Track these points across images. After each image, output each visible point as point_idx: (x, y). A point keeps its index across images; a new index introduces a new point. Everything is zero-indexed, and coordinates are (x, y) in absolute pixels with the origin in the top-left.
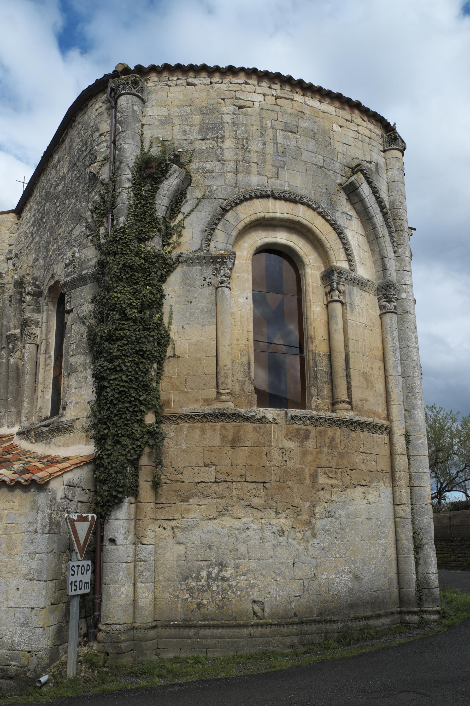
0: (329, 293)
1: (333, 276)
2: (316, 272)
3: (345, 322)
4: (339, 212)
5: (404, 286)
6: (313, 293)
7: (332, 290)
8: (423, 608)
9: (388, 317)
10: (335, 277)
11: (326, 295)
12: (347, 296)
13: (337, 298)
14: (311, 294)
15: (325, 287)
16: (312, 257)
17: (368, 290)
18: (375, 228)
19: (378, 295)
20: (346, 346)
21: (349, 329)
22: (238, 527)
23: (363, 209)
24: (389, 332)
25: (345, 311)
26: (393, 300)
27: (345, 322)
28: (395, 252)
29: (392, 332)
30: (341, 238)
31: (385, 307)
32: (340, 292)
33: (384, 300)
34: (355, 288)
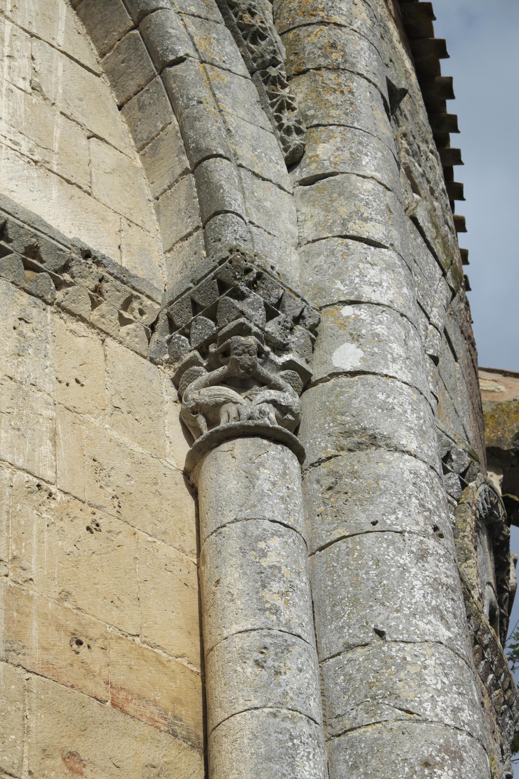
5: (347, 311)
8: (513, 650)
9: (229, 462)
17: (84, 307)
28: (293, 162)
31: (212, 411)
33: (206, 375)
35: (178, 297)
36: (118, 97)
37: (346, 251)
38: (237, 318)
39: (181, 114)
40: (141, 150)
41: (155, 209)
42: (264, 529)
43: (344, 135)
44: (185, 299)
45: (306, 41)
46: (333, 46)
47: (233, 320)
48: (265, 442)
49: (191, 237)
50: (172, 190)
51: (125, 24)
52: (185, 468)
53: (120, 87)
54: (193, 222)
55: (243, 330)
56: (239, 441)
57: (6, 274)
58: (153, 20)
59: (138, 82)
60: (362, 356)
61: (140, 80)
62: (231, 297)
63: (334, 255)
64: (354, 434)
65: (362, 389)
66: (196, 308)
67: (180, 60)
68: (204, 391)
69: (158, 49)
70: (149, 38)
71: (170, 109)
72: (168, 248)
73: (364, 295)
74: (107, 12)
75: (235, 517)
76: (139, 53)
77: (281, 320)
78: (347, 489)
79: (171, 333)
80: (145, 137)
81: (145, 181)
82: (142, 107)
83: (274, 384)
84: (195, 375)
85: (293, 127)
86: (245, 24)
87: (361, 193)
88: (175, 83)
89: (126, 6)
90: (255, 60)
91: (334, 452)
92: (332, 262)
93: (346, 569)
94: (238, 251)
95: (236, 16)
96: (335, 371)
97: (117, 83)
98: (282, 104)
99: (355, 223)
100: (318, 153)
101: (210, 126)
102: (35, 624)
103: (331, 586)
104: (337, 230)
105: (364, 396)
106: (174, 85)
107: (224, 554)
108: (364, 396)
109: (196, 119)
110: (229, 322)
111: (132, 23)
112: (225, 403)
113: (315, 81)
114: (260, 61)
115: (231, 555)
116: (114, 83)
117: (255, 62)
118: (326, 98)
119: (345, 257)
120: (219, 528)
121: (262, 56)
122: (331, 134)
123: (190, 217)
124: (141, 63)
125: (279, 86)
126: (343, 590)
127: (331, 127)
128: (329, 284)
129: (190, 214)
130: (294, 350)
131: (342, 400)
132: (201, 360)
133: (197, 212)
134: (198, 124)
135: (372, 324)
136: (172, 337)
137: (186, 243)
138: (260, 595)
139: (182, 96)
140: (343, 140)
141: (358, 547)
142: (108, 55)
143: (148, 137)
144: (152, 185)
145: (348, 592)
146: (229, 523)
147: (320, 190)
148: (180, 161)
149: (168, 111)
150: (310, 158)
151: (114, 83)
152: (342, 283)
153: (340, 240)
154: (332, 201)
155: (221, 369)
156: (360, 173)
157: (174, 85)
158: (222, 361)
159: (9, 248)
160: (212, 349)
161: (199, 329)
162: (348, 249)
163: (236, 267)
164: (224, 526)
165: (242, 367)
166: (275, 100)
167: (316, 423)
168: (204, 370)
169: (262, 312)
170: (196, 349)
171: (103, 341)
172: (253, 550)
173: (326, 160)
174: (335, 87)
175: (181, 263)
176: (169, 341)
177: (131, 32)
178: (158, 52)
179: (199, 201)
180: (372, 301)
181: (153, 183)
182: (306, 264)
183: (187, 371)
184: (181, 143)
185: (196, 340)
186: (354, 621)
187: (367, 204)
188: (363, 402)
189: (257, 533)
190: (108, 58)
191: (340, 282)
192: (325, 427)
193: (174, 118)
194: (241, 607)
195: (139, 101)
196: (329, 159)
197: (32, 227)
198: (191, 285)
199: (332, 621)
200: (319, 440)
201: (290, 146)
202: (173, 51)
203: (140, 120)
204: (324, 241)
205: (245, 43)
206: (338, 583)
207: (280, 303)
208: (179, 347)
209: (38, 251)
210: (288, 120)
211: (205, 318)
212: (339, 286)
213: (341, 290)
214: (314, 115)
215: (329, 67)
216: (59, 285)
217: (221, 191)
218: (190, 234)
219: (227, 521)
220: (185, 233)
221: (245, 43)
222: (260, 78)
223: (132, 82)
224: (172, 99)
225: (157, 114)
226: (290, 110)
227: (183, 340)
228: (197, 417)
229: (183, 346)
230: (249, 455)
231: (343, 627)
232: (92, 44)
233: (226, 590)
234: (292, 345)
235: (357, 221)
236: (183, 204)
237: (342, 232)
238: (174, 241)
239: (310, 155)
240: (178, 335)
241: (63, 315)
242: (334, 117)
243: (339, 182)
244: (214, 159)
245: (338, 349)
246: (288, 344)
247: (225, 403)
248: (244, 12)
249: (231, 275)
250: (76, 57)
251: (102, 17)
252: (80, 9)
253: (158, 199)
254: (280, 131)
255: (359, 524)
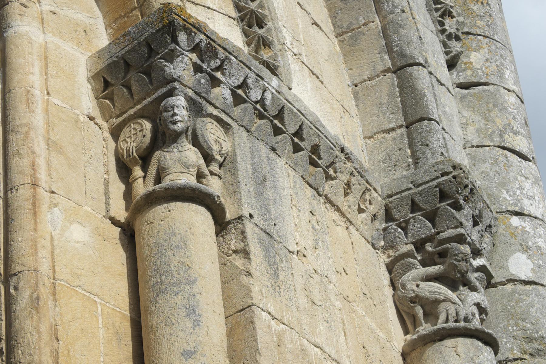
0: (145, 160)
1: (171, 57)
2: (69, 48)
5: (515, 221)
10: (182, 68)
11: (124, 170)
12: (247, 186)
13: (188, 179)
15: (116, 133)
19: (391, 246)
22: (263, 227)
25: (239, 262)
26: (473, 276)
28: (451, 65)
31: (431, 307)
32: (208, 158)
34: (281, 163)
35: (397, 193)
37: (507, 162)
38: (456, 227)
40: (340, 36)
43: (490, 46)
48: (480, 344)
49: (394, 132)
50: (373, 82)
52: (402, 350)
54: (397, 120)
56: (461, 340)
57: (299, 169)
60: (532, 267)
62: (451, 207)
63: (498, 165)
64: (534, 341)
66: (414, 207)
68: (422, 284)
71: (374, 9)
72: (369, 135)
73: (525, 208)
77: (480, 229)
81: (343, 66)
83: (473, 286)
84: (409, 267)
85: (454, 34)
87: (508, 106)
92: (496, 171)
96: (512, 278)
98: (445, 11)
100: (472, 60)
101: (412, 35)
104: (497, 140)
105: (539, 306)
108: (539, 306)
109: (400, 26)
110: (448, 229)
112: (444, 301)
118: (472, 7)
119: (506, 168)
122: (480, 44)
123: (392, 113)
127: (479, 37)
128: (497, 192)
129: (393, 111)
130: (485, 255)
131: (522, 307)
132: (416, 254)
133: (401, 111)
135: (535, 237)
136: (388, 227)
140: (490, 51)
143: (349, 28)
144: (350, 71)
148: (382, 59)
150: (466, 64)
152: (507, 193)
153: (501, 151)
155: (437, 267)
156: (506, 87)
158: (437, 260)
159: (302, 146)
160: (429, 247)
161: (417, 227)
162: (508, 161)
165: (460, 272)
166: (439, 6)
167: (500, 323)
169: (471, 223)
170: (412, 243)
173: (478, 69)
175: (384, 153)
176: (385, 230)
181: (351, 69)
182: (473, 167)
183: (402, 261)
185: (413, 236)
188: (538, 311)
191: (505, 192)
192: (509, 330)
193: (377, 18)
197: (315, 127)
198: (411, 186)
200: (505, 340)
201: (451, 52)
203: (341, 9)
204: (487, 148)
207: (480, 216)
209: (318, 149)
210: (450, 26)
211: (424, 219)
212: (505, 196)
213: (507, 200)
214: (464, 22)
216: (328, 177)
217: (425, 99)
218: (393, 129)
220: (387, 127)
225: (359, 9)
226: (450, 17)
228: (415, 306)
229: (399, 238)
230: (471, 355)
235: (510, 134)
236: (385, 100)
237: (501, 143)
240: (394, 227)
241: (327, 205)
242: (480, 28)
243: (492, 93)
244: (417, 67)
245: (512, 257)
246: (481, 250)
247: (444, 301)
249: (454, 189)
254: (442, 35)
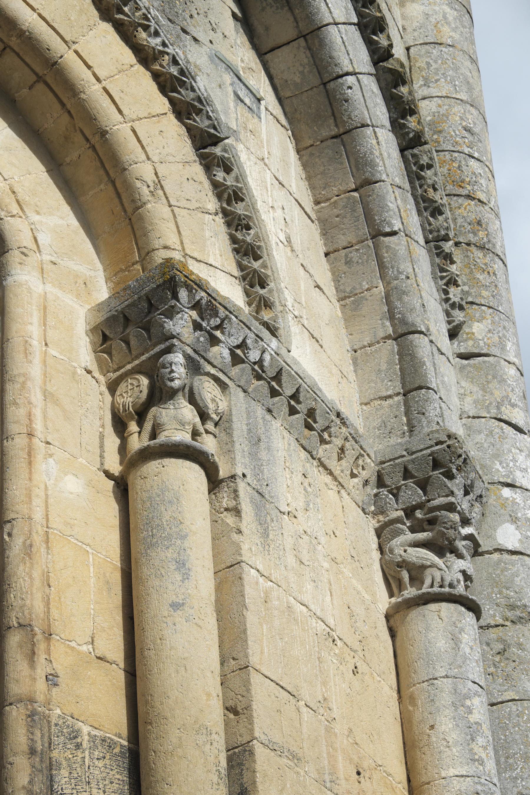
0: (141, 415)
1: (171, 313)
2: (68, 300)
3: (228, 573)
4: (205, 50)
5: (506, 492)
6: (46, 394)
7: (160, 393)
11: (120, 425)
12: (241, 446)
13: (183, 437)
14: (37, 397)
15: (112, 387)
16: (53, 221)
17: (332, 463)
18: (366, 183)
19: (381, 511)
20: (236, 710)
21: (252, 619)
23: (316, 81)
24: (445, 698)
25: (230, 519)
26: (461, 544)
27: (228, 573)
28: (453, 334)
29: (460, 701)
30: (209, 163)
31: (417, 573)
32: (204, 416)
35: (390, 460)
36: (325, 245)
38: (447, 496)
39: (389, 283)
41: (352, 360)
42: (469, 689)
44: (398, 464)
45: (457, 213)
46: (479, 223)
47: (443, 496)
48: (463, 609)
49: (391, 400)
50: (373, 348)
51: (347, 184)
53: (330, 237)
54: (395, 387)
55: (451, 507)
56: (444, 605)
58: (376, 191)
59: (349, 239)
61: (351, 238)
62: (444, 476)
64: (517, 609)
65: (521, 568)
67: (394, 233)
68: (410, 550)
69: (376, 218)
70: (368, 205)
71: (378, 275)
72: (366, 401)
74: (330, 167)
75: (445, 673)
76: (356, 215)
78: (515, 658)
79: (378, 488)
80: (348, 290)
82: (349, 262)
83: (460, 554)
84: (398, 533)
86: (429, 198)
88: (387, 253)
89: (350, 168)
90: (431, 232)
91: (501, 621)
93: (517, 729)
94: (456, 439)
95: (421, 187)
96: (499, 547)
97: (327, 232)
98: (450, 279)
99: (506, 407)
100: (474, 331)
102: (340, 758)
103: (504, 740)
104: (494, 412)
106: (386, 255)
107: (437, 704)
108: (523, 575)
109: (404, 293)
110: (439, 497)
111: (354, 187)
112: (430, 566)
113: (467, 256)
114: (435, 234)
115: (444, 706)
116: (324, 232)
117: (431, 233)
120: (431, 679)
121: (439, 231)
123: (390, 381)
124: (356, 224)
125: (449, 262)
126: (515, 746)
127: (483, 308)
129: (391, 378)
131: (507, 576)
133: (399, 379)
134: (406, 298)
136: (380, 492)
137: (386, 403)
138: (470, 747)
139: (392, 267)
140: (493, 322)
141: (526, 712)
142: (323, 205)
145: (520, 749)
146: (441, 677)
147: (477, 368)
149: (375, 276)
150: (467, 334)
151: (324, 232)
152: (500, 464)
153: (497, 423)
154: (488, 382)
155: (425, 534)
157: (386, 255)
158: (426, 527)
160: (419, 514)
161: (408, 494)
163: (453, 453)
164: (436, 679)
165: (448, 539)
166: (445, 274)
167: (484, 590)
168: (407, 530)
170: (402, 509)
171: (339, 492)
172: (462, 706)
173: (480, 340)
174: (483, 266)
176: (376, 495)
177: (352, 193)
178: (375, 220)
179: (401, 369)
180: (523, 486)
181: (351, 335)
182: (468, 437)
183: (391, 527)
184: (386, 309)
186: (526, 776)
187: (513, 390)
188: (523, 581)
189: (465, 691)
190: (323, 208)
191: (498, 464)
193: (381, 284)
194: (457, 754)
195: (346, 256)
196: (483, 339)
198: (405, 453)
199: (506, 770)
202: (390, 224)
203: (345, 273)
204: (483, 420)
205: (425, 214)
206: (510, 739)
207: (472, 486)
208: (386, 504)
209: (314, 413)
213: (499, 471)
215: (477, 244)
216: (323, 441)
217: (425, 367)
218: (390, 397)
219: (439, 676)
220: (385, 394)
221: (425, 214)
222: (434, 249)
223: (343, 237)
224: (382, 266)
225: (364, 274)
227: (391, 499)
230: (453, 619)
231: (516, 778)
232: (309, 190)
233: (442, 736)
234: (473, 521)
236: (384, 367)
238: (372, 397)
239: (467, 331)
240: (386, 493)
247: (430, 566)
248: (429, 186)
249: (448, 458)
250: (303, 205)
251: (324, 170)
252: (303, 155)
253: (355, 352)
255: (526, 691)
